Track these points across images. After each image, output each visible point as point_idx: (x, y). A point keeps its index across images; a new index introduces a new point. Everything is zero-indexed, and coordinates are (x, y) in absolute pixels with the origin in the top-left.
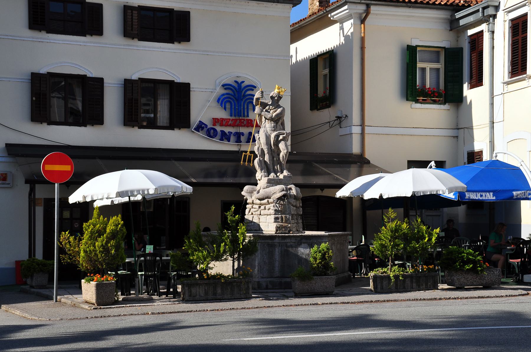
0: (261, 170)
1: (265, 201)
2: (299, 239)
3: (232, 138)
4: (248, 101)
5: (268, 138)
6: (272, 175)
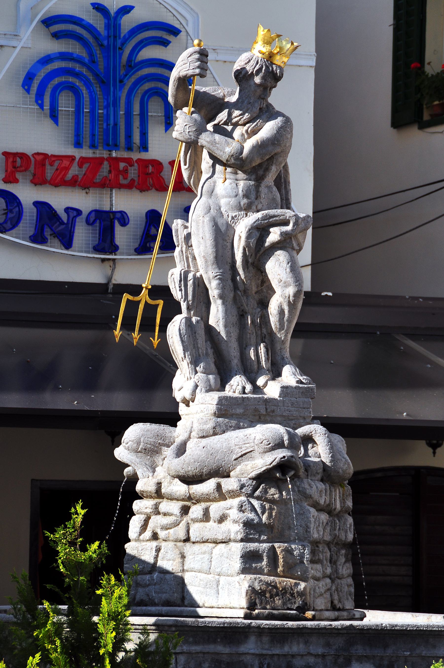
0: (195, 363)
1: (208, 486)
2: (340, 641)
3: (82, 234)
4: (147, 86)
5: (222, 236)
6: (237, 385)
